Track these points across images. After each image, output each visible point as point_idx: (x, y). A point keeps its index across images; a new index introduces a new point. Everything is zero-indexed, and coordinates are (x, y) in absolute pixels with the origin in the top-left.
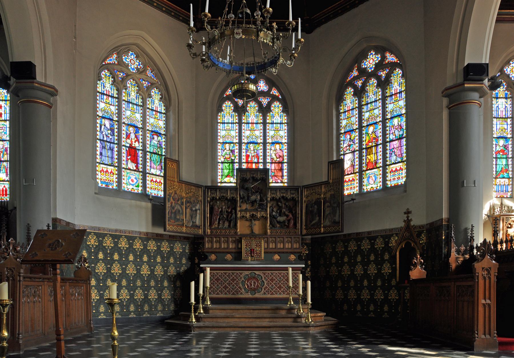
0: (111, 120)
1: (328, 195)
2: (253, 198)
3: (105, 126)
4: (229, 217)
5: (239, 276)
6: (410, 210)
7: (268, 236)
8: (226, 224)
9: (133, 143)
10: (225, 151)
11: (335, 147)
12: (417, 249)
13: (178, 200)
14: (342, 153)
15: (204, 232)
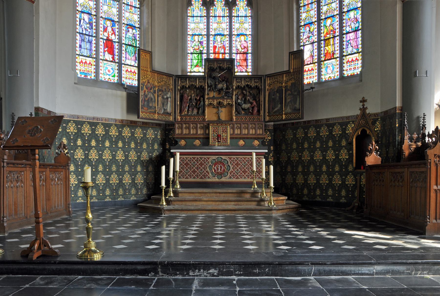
0: (90, 14)
1: (289, 84)
2: (220, 86)
3: (84, 20)
4: (198, 104)
5: (207, 160)
6: (365, 99)
7: (234, 123)
8: (195, 111)
9: (110, 36)
10: (195, 42)
11: (295, 39)
12: (372, 136)
13: (151, 89)
14: (302, 44)
15: (175, 118)
